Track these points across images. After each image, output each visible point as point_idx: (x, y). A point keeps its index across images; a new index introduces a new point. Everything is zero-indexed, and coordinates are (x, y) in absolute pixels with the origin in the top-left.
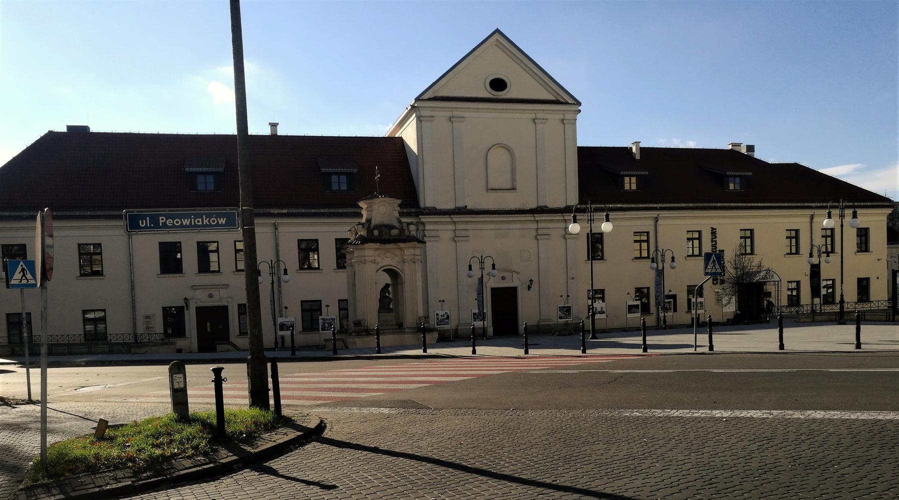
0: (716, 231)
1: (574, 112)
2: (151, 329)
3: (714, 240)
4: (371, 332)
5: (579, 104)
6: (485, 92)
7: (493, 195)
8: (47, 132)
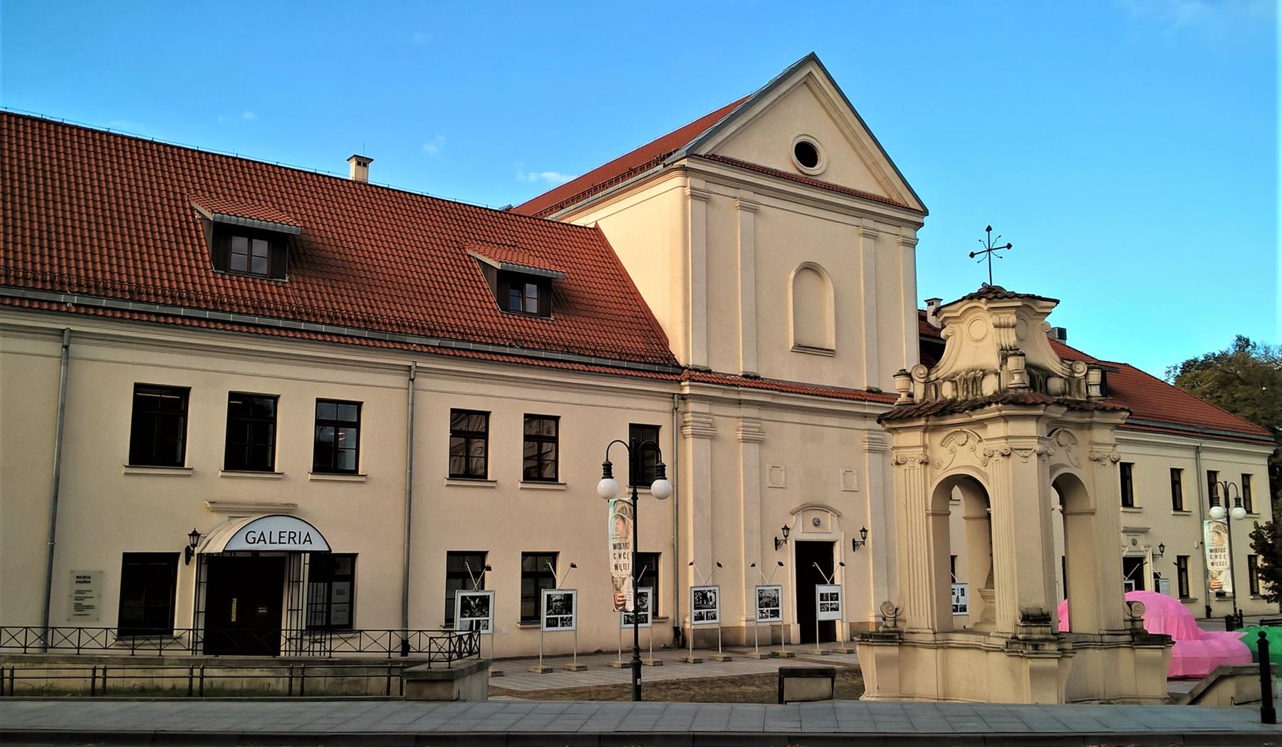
5: (925, 212)
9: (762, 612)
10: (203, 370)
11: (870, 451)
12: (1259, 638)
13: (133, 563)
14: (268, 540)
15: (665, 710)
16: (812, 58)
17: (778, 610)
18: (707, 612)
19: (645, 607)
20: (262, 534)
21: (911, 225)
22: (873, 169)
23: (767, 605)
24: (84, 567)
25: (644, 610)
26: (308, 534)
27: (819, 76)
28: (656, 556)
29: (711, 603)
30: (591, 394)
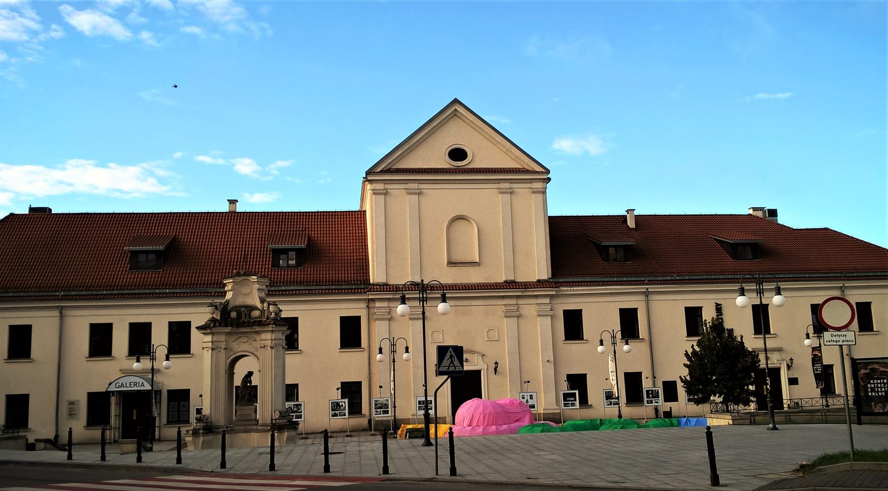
0: (721, 307)
1: (543, 180)
2: (74, 416)
3: (719, 317)
4: (214, 430)
5: (548, 172)
6: (445, 162)
7: (454, 270)
8: (7, 214)
9: (377, 411)
10: (288, 311)
11: (506, 317)
12: (707, 431)
13: (92, 397)
14: (125, 386)
15: (360, 459)
16: (456, 101)
17: (388, 411)
18: (340, 413)
19: (300, 411)
20: (122, 384)
21: (541, 181)
22: (507, 153)
23: (380, 408)
24: (72, 398)
25: (299, 412)
26: (143, 383)
27: (461, 109)
28: (831, 366)
29: (342, 408)
30: (83, 310)
